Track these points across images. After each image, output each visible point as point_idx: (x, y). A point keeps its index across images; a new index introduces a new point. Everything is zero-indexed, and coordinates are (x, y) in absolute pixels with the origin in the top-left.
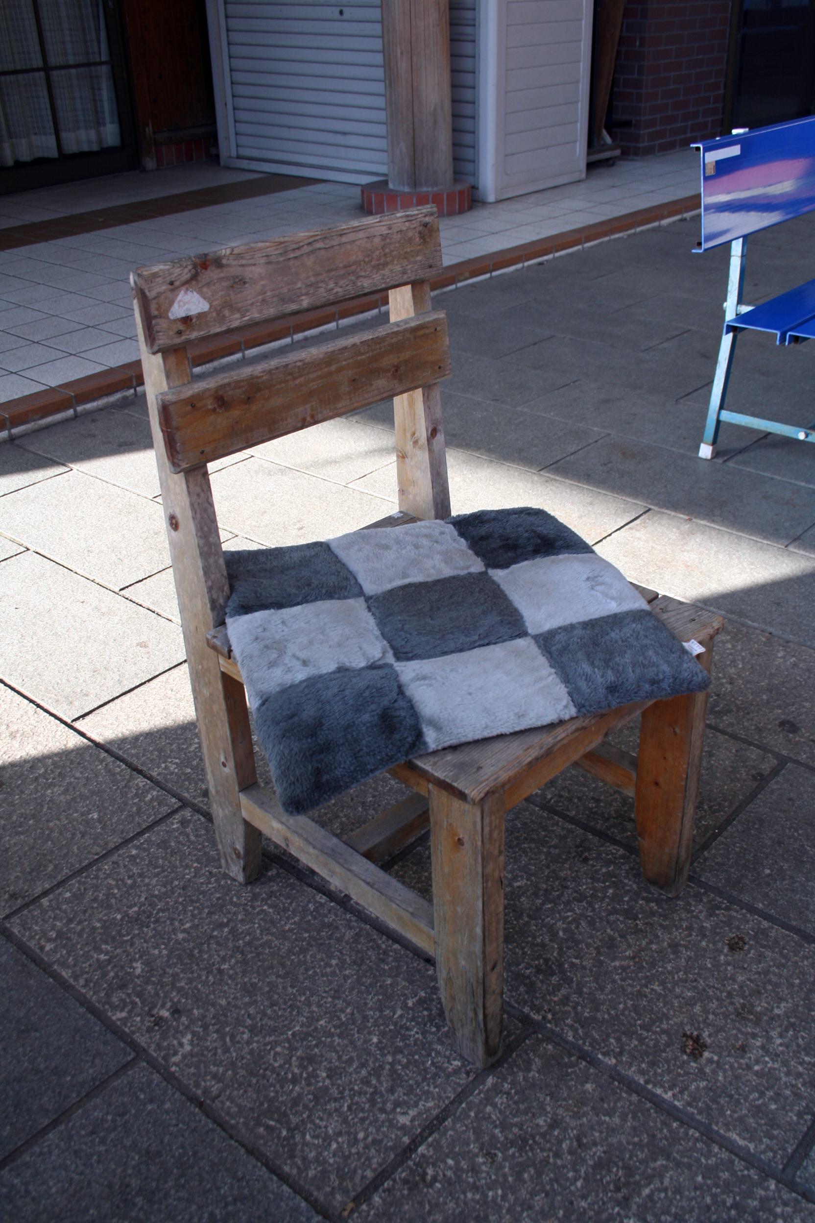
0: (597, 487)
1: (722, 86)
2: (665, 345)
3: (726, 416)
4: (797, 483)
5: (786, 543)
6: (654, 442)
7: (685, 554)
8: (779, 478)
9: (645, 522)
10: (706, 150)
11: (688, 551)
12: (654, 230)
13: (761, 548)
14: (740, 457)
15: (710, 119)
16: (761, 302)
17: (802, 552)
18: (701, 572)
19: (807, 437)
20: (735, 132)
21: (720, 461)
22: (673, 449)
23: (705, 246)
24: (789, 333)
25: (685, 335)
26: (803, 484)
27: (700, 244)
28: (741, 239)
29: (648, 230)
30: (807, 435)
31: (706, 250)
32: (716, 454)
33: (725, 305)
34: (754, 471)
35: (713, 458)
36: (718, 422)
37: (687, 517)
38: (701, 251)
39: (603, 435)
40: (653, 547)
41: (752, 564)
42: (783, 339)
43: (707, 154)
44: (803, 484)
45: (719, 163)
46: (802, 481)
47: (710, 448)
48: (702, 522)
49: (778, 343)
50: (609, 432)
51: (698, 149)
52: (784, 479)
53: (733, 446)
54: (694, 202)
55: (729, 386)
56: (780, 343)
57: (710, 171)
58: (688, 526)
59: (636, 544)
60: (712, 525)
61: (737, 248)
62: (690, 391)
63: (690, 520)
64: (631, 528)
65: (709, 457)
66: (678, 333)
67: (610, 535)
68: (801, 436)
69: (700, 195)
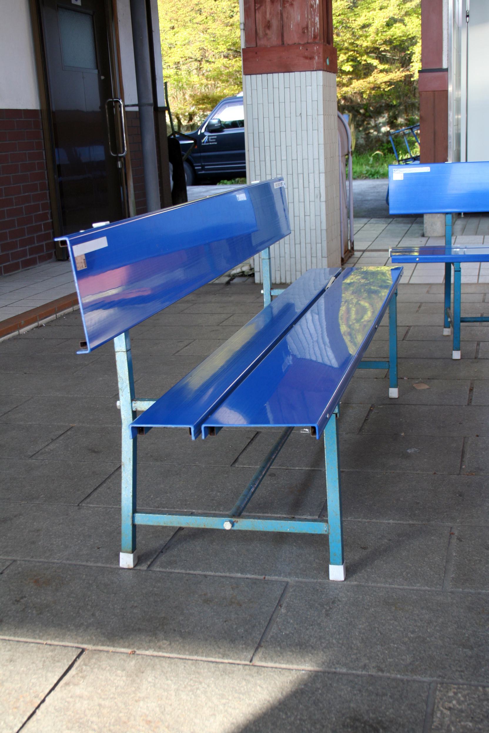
0: (15, 635)
1: (49, 216)
2: (52, 447)
3: (142, 519)
4: (232, 575)
5: (249, 657)
6: (67, 559)
7: (141, 703)
8: (212, 574)
9: (81, 671)
10: (73, 243)
11: (143, 699)
12: (14, 338)
13: (224, 671)
14: (163, 558)
15: (44, 243)
16: (159, 397)
17: (270, 664)
18: (168, 727)
19: (233, 525)
20: (95, 225)
21: (144, 567)
22: (89, 564)
23: (90, 346)
24: (203, 426)
25: (69, 433)
26: (239, 575)
27: (84, 344)
28: (123, 334)
29: (9, 339)
30: (233, 524)
31: (92, 350)
32: (138, 561)
33: (118, 403)
34: (183, 571)
35: (135, 566)
36: (134, 526)
37: (129, 651)
38: (87, 352)
39: (8, 563)
40: (100, 705)
41: (222, 696)
42: (198, 432)
43: (74, 247)
44: (239, 575)
45: (89, 256)
46: (237, 572)
47: (131, 556)
48: (147, 653)
49: (193, 438)
50: (14, 558)
51: (64, 243)
52: (217, 574)
53: (151, 549)
54: (72, 299)
55: (138, 488)
56: (196, 438)
57: (82, 265)
58: (133, 663)
59: (78, 705)
60: (160, 654)
61: (120, 344)
62: (90, 492)
63: (134, 653)
64: (67, 684)
65: (132, 566)
66: (61, 432)
67: (43, 701)
68: (227, 526)
69: (75, 294)
